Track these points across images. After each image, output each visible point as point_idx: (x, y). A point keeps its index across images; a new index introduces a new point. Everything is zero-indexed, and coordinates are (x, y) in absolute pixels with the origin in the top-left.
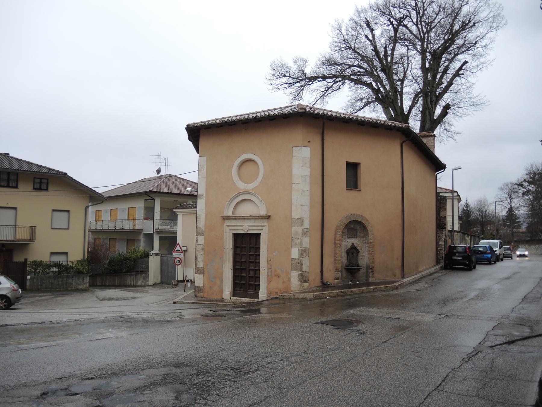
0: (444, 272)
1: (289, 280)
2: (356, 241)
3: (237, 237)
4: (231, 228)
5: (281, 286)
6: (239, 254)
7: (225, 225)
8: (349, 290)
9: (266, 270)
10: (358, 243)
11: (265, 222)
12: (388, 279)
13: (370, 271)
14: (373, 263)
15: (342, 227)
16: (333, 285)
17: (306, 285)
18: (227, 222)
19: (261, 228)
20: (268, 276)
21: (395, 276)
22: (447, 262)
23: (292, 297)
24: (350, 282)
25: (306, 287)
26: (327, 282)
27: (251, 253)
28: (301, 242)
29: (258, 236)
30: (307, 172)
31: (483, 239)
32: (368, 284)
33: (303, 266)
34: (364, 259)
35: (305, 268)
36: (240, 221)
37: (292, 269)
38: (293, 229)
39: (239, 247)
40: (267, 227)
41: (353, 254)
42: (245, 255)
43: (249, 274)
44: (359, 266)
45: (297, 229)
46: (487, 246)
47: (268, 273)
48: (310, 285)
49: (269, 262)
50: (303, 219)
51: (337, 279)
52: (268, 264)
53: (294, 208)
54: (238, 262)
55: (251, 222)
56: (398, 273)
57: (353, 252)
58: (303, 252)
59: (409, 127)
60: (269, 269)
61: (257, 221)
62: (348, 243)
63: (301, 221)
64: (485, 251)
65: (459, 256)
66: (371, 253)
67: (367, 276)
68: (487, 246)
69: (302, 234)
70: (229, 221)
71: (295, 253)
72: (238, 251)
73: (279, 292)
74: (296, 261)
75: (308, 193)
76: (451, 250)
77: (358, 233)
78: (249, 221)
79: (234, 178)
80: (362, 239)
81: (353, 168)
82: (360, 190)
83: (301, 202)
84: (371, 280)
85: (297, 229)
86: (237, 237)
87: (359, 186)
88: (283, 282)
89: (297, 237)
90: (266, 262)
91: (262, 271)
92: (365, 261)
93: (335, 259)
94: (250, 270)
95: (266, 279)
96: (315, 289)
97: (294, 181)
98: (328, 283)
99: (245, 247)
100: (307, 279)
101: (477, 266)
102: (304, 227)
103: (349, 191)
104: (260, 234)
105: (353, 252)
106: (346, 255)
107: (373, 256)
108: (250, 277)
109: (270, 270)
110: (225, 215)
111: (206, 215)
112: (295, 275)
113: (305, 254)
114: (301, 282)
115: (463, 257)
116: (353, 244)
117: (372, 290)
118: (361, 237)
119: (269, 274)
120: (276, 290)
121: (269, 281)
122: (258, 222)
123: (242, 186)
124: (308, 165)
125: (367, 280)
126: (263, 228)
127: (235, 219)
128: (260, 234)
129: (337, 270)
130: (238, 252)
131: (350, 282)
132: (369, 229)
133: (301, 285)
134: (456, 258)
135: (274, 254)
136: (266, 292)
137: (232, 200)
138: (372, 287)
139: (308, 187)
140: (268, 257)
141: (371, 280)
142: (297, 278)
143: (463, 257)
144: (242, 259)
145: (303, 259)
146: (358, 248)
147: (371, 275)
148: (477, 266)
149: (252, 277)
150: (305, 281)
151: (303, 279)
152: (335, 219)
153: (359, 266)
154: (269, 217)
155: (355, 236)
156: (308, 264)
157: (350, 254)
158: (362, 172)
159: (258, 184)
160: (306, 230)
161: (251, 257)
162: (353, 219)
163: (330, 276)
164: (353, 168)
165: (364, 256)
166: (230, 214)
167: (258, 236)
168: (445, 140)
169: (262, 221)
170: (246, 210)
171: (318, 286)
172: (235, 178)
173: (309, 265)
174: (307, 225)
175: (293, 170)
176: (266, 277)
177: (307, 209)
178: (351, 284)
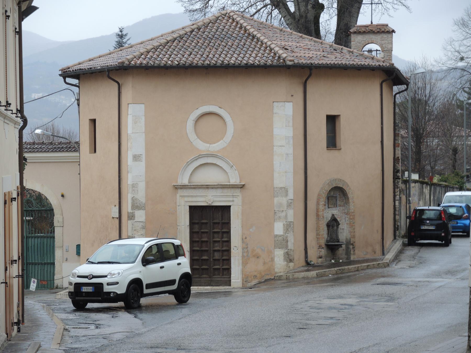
0: (411, 251)
1: (272, 260)
2: (335, 211)
3: (193, 210)
4: (186, 199)
5: (261, 267)
6: (198, 232)
7: (178, 195)
8: (346, 267)
9: (240, 250)
10: (338, 214)
11: (237, 192)
12: (368, 257)
13: (351, 247)
14: (354, 237)
15: (324, 196)
16: (316, 264)
17: (291, 264)
18: (181, 192)
19: (231, 199)
20: (243, 256)
21: (375, 253)
22: (413, 234)
23: (291, 277)
24: (333, 261)
25: (291, 268)
26: (311, 261)
27: (215, 230)
28: (286, 216)
29: (227, 209)
30: (290, 134)
31: (453, 189)
32: (350, 263)
33: (289, 243)
34: (344, 234)
35: (290, 246)
36: (201, 190)
37: (275, 247)
38: (276, 200)
39: (198, 223)
40: (240, 198)
41: (333, 227)
42: (207, 232)
43: (214, 256)
44: (338, 242)
45: (281, 200)
46: (463, 205)
47: (243, 253)
48: (295, 265)
49: (244, 240)
50: (287, 189)
51: (321, 257)
52: (243, 242)
53: (276, 175)
54: (196, 241)
55: (219, 192)
56: (378, 248)
57: (333, 224)
58: (288, 227)
59: (393, 64)
60: (245, 248)
61: (225, 191)
62: (328, 214)
63: (285, 191)
64: (460, 214)
65: (431, 225)
66: (352, 225)
67: (348, 253)
68: (463, 205)
69: (287, 207)
70: (185, 190)
71: (279, 228)
72: (196, 228)
73: (258, 275)
74: (280, 238)
75: (291, 157)
76: (417, 218)
77: (338, 202)
78: (214, 190)
79: (189, 135)
80: (341, 208)
81: (332, 120)
82: (340, 149)
83: (284, 170)
84: (352, 258)
85: (281, 200)
86: (193, 210)
87: (338, 144)
88: (264, 263)
89: (282, 209)
90: (240, 241)
91: (234, 252)
92: (345, 234)
93: (318, 234)
94: (215, 251)
95: (241, 261)
96: (300, 269)
97: (276, 143)
98: (312, 263)
99: (206, 223)
100: (292, 258)
101: (454, 240)
102: (288, 198)
103: (329, 151)
104: (230, 206)
105: (333, 224)
106: (326, 228)
107: (354, 229)
108: (215, 260)
109: (246, 250)
110: (180, 182)
111: (147, 183)
112: (279, 255)
113: (289, 230)
114: (287, 261)
115: (437, 226)
116: (333, 215)
117: (366, 267)
118: (340, 206)
119: (245, 254)
120: (255, 274)
121: (245, 263)
122: (228, 192)
123: (202, 146)
124: (291, 124)
125: (348, 258)
126: (235, 199)
127: (194, 188)
128: (230, 206)
129: (320, 247)
130: (196, 230)
131: (333, 261)
132: (350, 196)
133: (287, 265)
134: (426, 228)
135: (251, 230)
136: (240, 276)
137: (188, 164)
138: (366, 264)
139: (291, 151)
140: (243, 234)
141: (352, 258)
142: (282, 258)
143: (437, 226)
144: (222, 238)
145: (289, 235)
146: (338, 220)
147: (352, 252)
148: (454, 240)
149: (218, 260)
150: (291, 261)
151: (289, 258)
152: (318, 187)
153: (338, 242)
154: (243, 187)
155: (335, 205)
156: (293, 241)
157: (331, 227)
158: (341, 126)
159: (226, 145)
160: (290, 201)
161: (216, 235)
162: (334, 186)
163: (314, 254)
164: (332, 120)
165: (343, 229)
166: (185, 181)
167: (227, 209)
168: (391, 8)
169: (233, 190)
170: (209, 176)
171: (303, 266)
172: (192, 136)
173: (295, 242)
174: (291, 195)
175: (275, 130)
176: (241, 258)
177: (291, 175)
178: (333, 263)
